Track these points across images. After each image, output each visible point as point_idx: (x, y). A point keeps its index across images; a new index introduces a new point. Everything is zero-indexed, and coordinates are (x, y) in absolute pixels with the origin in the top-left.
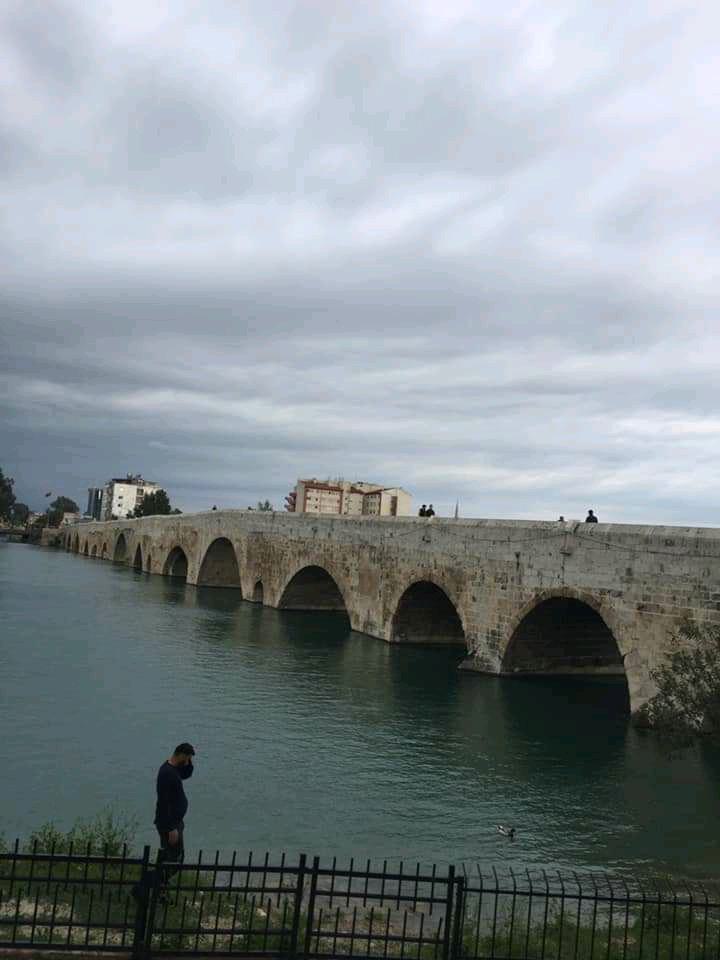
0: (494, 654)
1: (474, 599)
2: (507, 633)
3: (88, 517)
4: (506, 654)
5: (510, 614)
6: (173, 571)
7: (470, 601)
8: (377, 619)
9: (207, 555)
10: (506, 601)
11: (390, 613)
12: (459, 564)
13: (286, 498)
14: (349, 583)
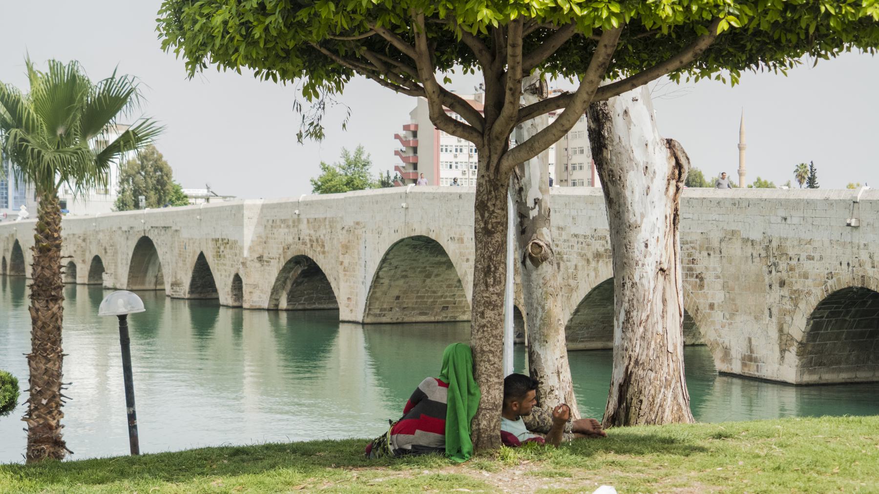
6: (289, 301)
9: (380, 268)
11: (792, 339)
13: (397, 136)
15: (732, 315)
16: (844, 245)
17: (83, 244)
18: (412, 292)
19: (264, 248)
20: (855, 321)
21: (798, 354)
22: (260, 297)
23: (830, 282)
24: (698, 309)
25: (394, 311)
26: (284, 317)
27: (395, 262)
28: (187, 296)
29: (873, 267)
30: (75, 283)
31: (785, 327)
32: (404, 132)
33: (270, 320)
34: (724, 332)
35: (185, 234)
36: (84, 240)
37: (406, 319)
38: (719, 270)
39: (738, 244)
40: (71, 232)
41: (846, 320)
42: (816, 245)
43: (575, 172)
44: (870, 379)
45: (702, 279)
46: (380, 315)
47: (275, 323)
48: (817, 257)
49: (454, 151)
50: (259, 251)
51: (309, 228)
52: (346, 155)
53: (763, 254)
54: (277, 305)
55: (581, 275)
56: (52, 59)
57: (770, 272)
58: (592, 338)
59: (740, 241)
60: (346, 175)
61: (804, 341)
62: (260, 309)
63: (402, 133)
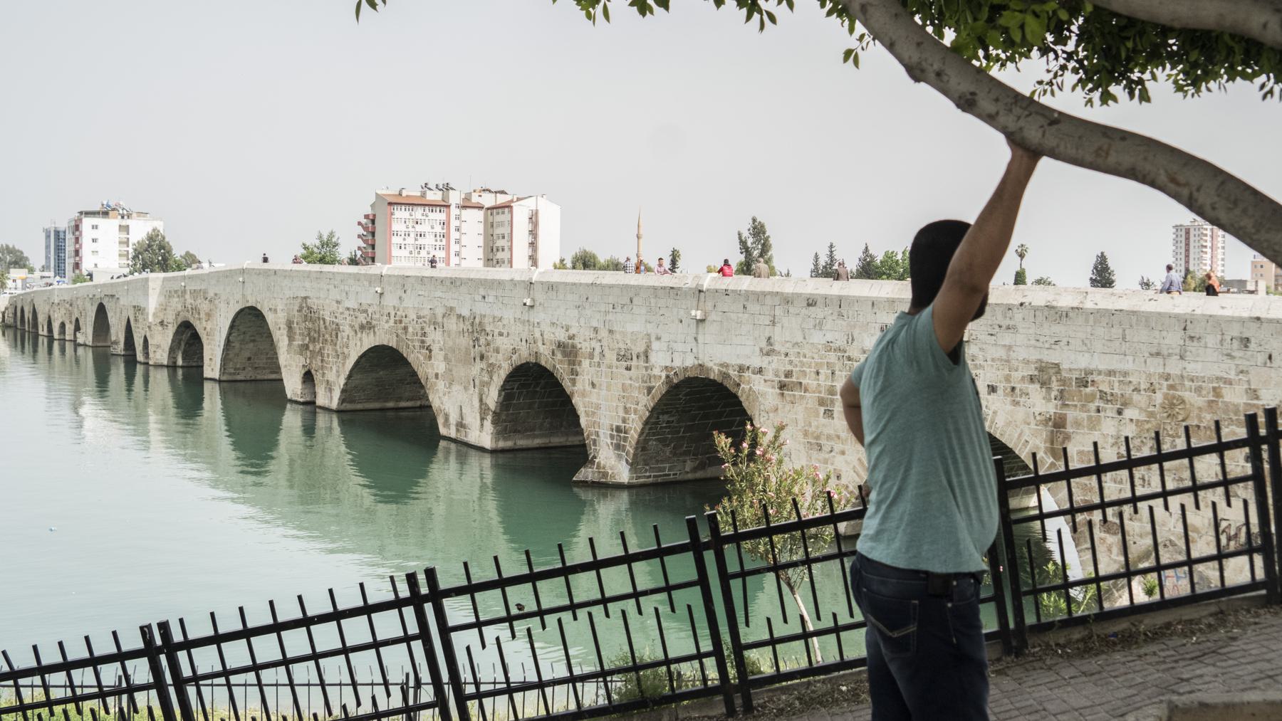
6: (184, 359)
9: (229, 334)
13: (359, 223)
17: (70, 308)
18: (261, 354)
20: (545, 392)
25: (247, 370)
26: (180, 372)
27: (242, 329)
28: (123, 353)
29: (543, 344)
31: (484, 397)
32: (365, 220)
33: (169, 376)
34: (445, 399)
36: (71, 305)
37: (259, 377)
39: (454, 319)
40: (62, 298)
41: (537, 392)
42: (505, 322)
43: (498, 253)
44: (564, 444)
45: (430, 351)
46: (234, 374)
48: (505, 334)
50: (161, 316)
52: (320, 237)
53: (470, 328)
54: (175, 363)
55: (352, 343)
57: (474, 346)
58: (368, 400)
59: (455, 317)
60: (320, 253)
61: (498, 411)
62: (162, 366)
63: (364, 221)
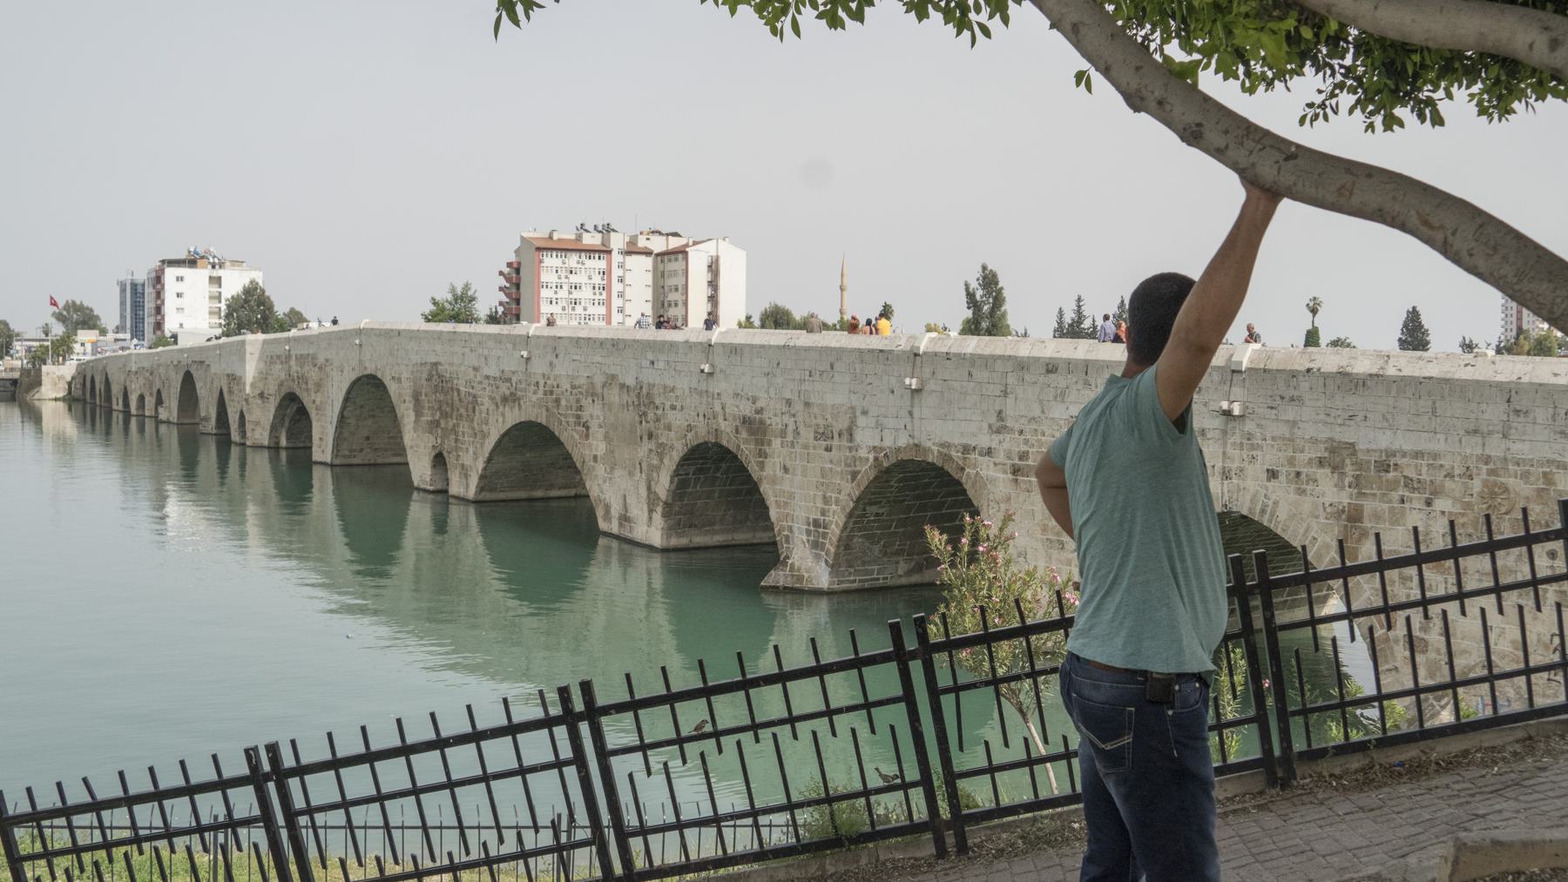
0: (817, 557)
1: (786, 470)
2: (836, 520)
3: (121, 336)
4: (837, 555)
5: (839, 493)
6: (288, 439)
7: (779, 473)
8: (638, 511)
9: (344, 408)
10: (831, 469)
11: (659, 498)
12: (759, 411)
13: (501, 273)
14: (590, 449)
15: (612, 469)
16: (700, 393)
19: (265, 385)
20: (727, 478)
21: (664, 516)
22: (261, 435)
23: (690, 435)
24: (584, 462)
26: (283, 455)
28: (214, 431)
29: (725, 420)
30: (144, 416)
34: (606, 487)
35: (213, 370)
36: (151, 374)
37: (380, 461)
38: (602, 418)
39: (616, 390)
41: (717, 477)
42: (678, 393)
44: (751, 541)
45: (588, 428)
47: (274, 460)
49: (554, 287)
51: (297, 365)
52: (453, 290)
54: (278, 443)
56: (606, 223)
57: (641, 422)
60: (453, 310)
61: (670, 501)
62: (262, 447)
